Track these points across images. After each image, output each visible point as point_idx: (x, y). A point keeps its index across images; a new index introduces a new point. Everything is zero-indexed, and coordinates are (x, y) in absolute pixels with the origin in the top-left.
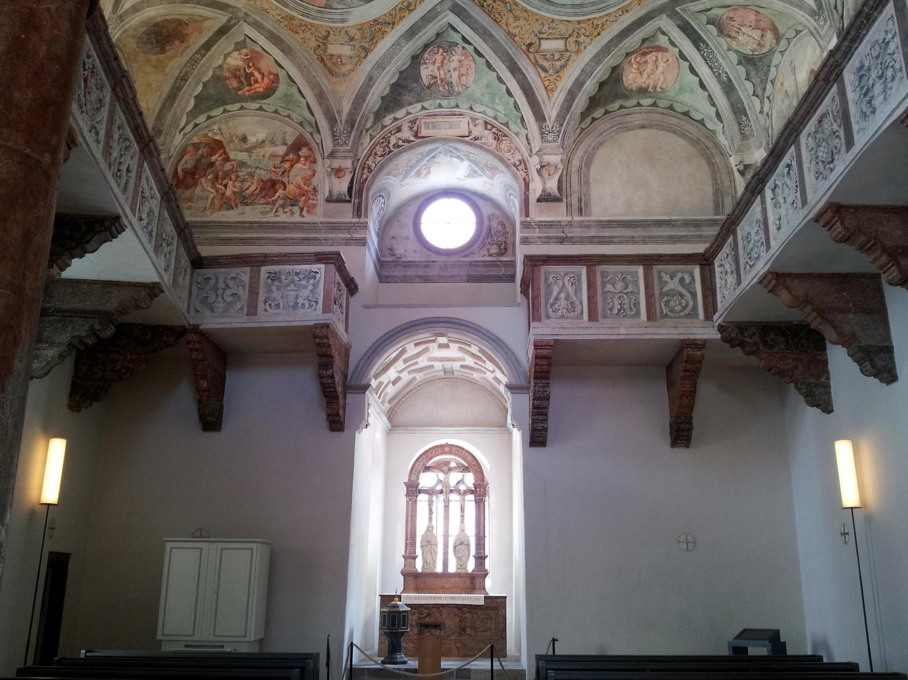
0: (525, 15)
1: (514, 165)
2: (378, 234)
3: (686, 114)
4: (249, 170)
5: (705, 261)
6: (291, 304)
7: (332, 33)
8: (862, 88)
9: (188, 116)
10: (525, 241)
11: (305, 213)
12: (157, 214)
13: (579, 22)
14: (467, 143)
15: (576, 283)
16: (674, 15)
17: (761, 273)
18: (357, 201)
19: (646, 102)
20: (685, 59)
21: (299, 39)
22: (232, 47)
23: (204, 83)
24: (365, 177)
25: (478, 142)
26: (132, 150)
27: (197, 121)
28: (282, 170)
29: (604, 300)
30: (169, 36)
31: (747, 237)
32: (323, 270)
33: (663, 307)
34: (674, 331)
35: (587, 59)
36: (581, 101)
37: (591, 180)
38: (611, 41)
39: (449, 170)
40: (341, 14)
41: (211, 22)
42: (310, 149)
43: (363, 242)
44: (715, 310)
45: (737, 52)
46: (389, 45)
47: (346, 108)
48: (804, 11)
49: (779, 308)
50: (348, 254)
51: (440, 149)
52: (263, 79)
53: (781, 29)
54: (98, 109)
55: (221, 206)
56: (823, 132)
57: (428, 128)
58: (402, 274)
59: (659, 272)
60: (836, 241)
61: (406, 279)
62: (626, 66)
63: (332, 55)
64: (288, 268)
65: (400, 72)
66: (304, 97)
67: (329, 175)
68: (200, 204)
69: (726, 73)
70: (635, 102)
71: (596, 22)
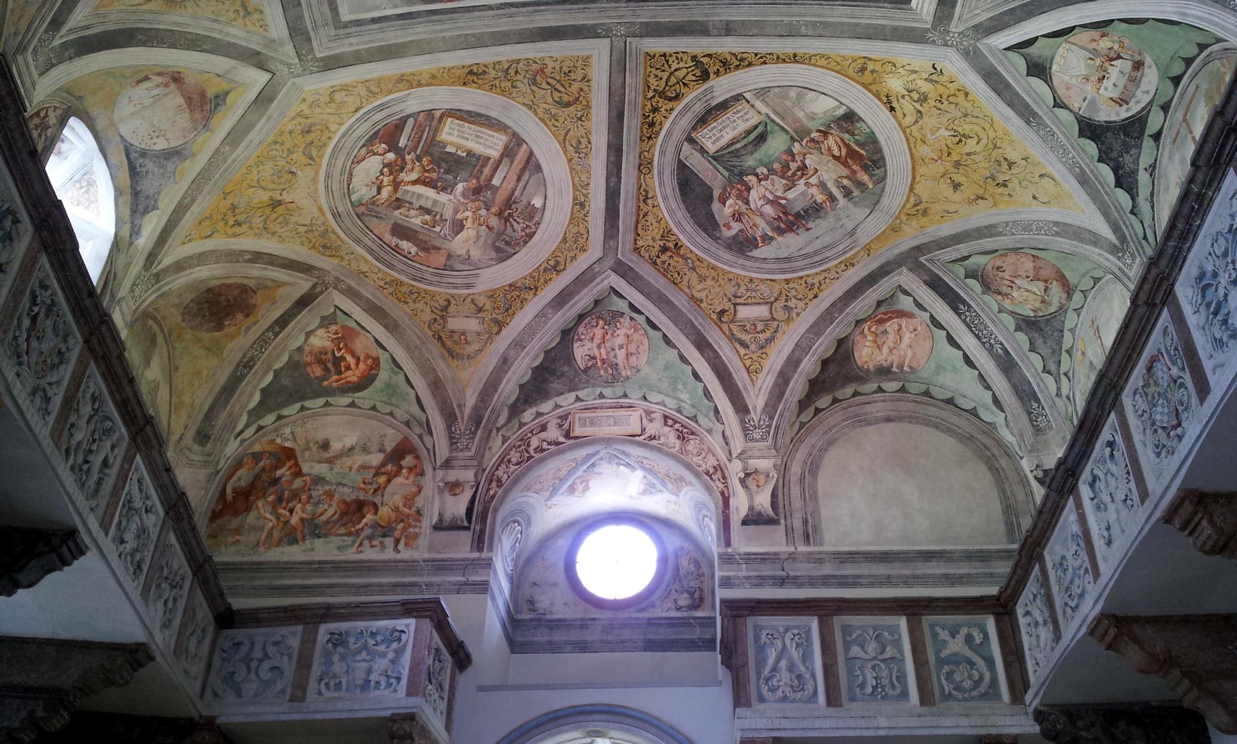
0: (714, 274)
1: (707, 473)
2: (511, 579)
3: (950, 401)
4: (327, 488)
5: (1002, 607)
6: (360, 682)
7: (453, 302)
8: (1208, 305)
9: (249, 416)
10: (726, 582)
11: (401, 546)
12: (154, 537)
13: (788, 281)
14: (640, 444)
15: (804, 644)
16: (918, 268)
17: (1090, 618)
18: (478, 528)
19: (891, 386)
20: (941, 327)
21: (408, 310)
22: (317, 322)
23: (275, 371)
24: (492, 493)
25: (654, 442)
26: (117, 435)
27: (262, 422)
28: (375, 486)
29: (850, 671)
30: (229, 306)
31: (1061, 564)
32: (412, 628)
33: (944, 683)
34: (964, 721)
35: (802, 329)
36: (797, 387)
37: (820, 493)
38: (834, 304)
39: (616, 486)
40: (466, 277)
41: (288, 288)
42: (417, 457)
43: (483, 588)
44: (1026, 686)
45: (1012, 313)
46: (530, 316)
47: (471, 400)
48: (1101, 248)
49: (1126, 678)
50: (454, 607)
51: (601, 454)
52: (357, 364)
53: (1072, 278)
54: (54, 367)
55: (281, 540)
56: (1156, 384)
57: (584, 425)
58: (546, 639)
59: (932, 626)
60: (1206, 552)
61: (553, 648)
62: (858, 338)
63: (453, 332)
64: (361, 625)
65: (546, 352)
66: (412, 387)
67: (441, 491)
68: (252, 538)
69: (1001, 344)
70: (874, 386)
71: (810, 281)
